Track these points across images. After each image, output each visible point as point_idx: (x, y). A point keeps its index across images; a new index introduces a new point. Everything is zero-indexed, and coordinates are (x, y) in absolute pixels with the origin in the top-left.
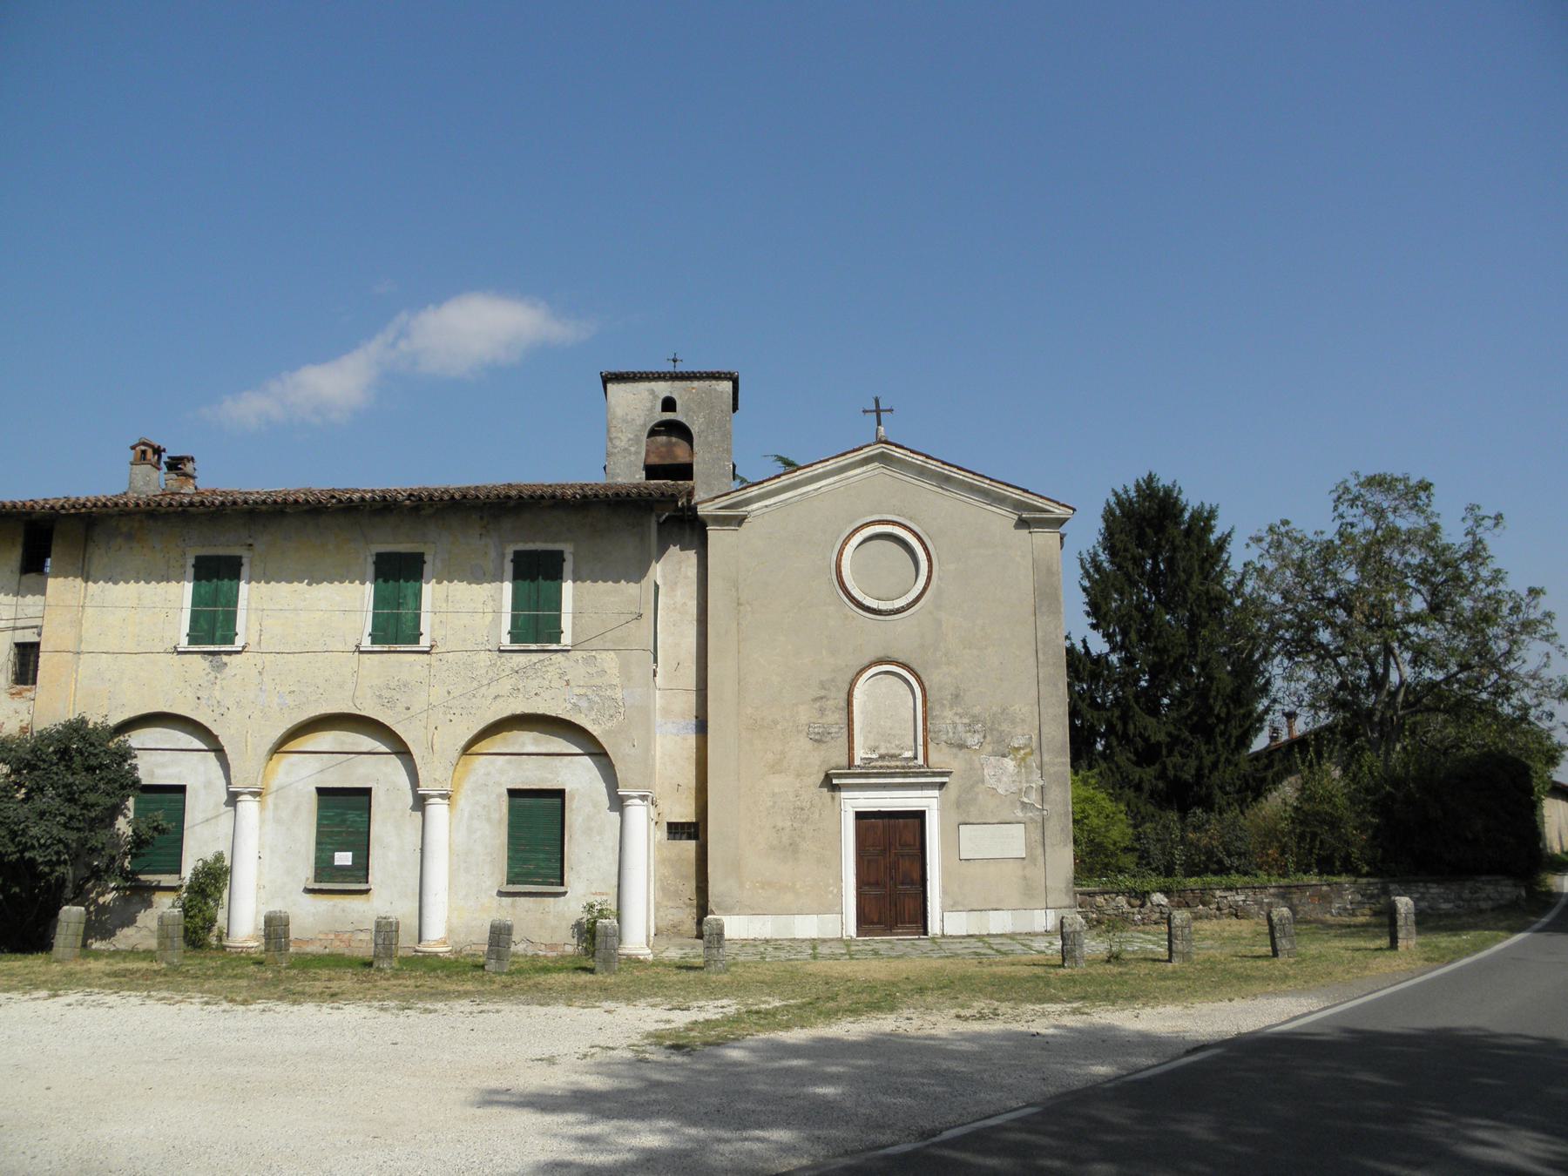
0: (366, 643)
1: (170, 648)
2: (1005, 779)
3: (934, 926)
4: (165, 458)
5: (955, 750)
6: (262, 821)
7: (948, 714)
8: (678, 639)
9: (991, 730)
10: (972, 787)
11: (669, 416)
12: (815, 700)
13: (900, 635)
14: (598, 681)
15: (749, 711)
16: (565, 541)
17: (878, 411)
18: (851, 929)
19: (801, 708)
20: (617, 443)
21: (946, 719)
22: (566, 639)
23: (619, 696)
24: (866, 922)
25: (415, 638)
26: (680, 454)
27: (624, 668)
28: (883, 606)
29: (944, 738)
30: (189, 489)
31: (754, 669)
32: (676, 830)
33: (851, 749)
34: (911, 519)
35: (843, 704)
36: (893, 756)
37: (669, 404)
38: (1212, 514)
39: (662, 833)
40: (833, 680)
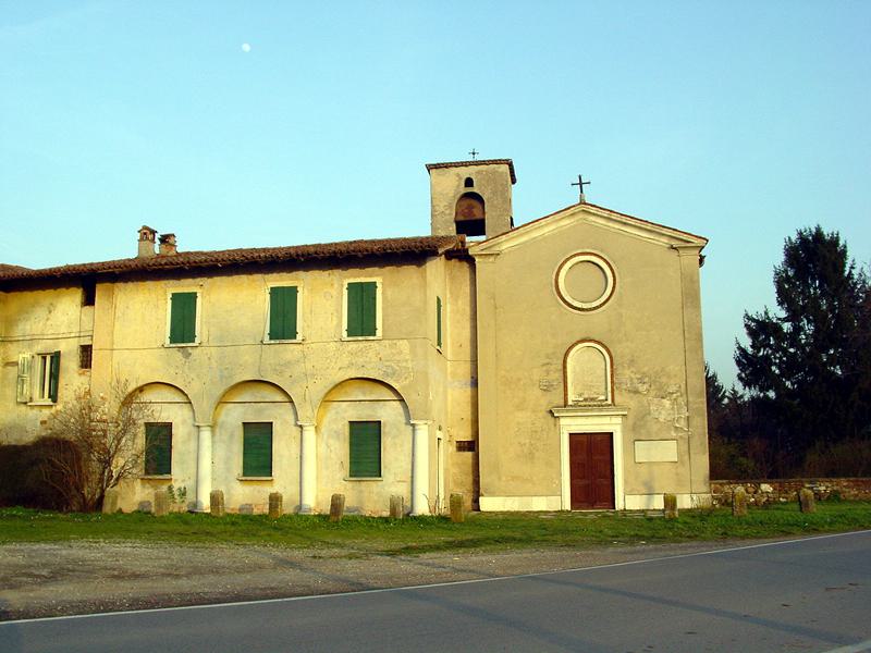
0: (267, 339)
1: (159, 344)
2: (663, 412)
3: (619, 505)
4: (158, 236)
5: (632, 394)
6: (213, 442)
7: (627, 372)
8: (456, 331)
9: (655, 382)
10: (643, 417)
11: (469, 190)
12: (544, 365)
13: (597, 323)
14: (397, 358)
15: (503, 372)
16: (377, 276)
17: (581, 184)
18: (567, 506)
19: (535, 371)
20: (437, 208)
21: (626, 374)
22: (379, 333)
23: (410, 366)
24: (576, 500)
25: (293, 335)
26: (477, 215)
27: (413, 351)
28: (585, 306)
29: (625, 387)
30: (172, 253)
31: (508, 348)
32: (463, 446)
33: (566, 395)
34: (602, 251)
35: (561, 367)
36: (592, 399)
37: (469, 182)
38: (838, 239)
39: (453, 448)
40: (554, 353)
